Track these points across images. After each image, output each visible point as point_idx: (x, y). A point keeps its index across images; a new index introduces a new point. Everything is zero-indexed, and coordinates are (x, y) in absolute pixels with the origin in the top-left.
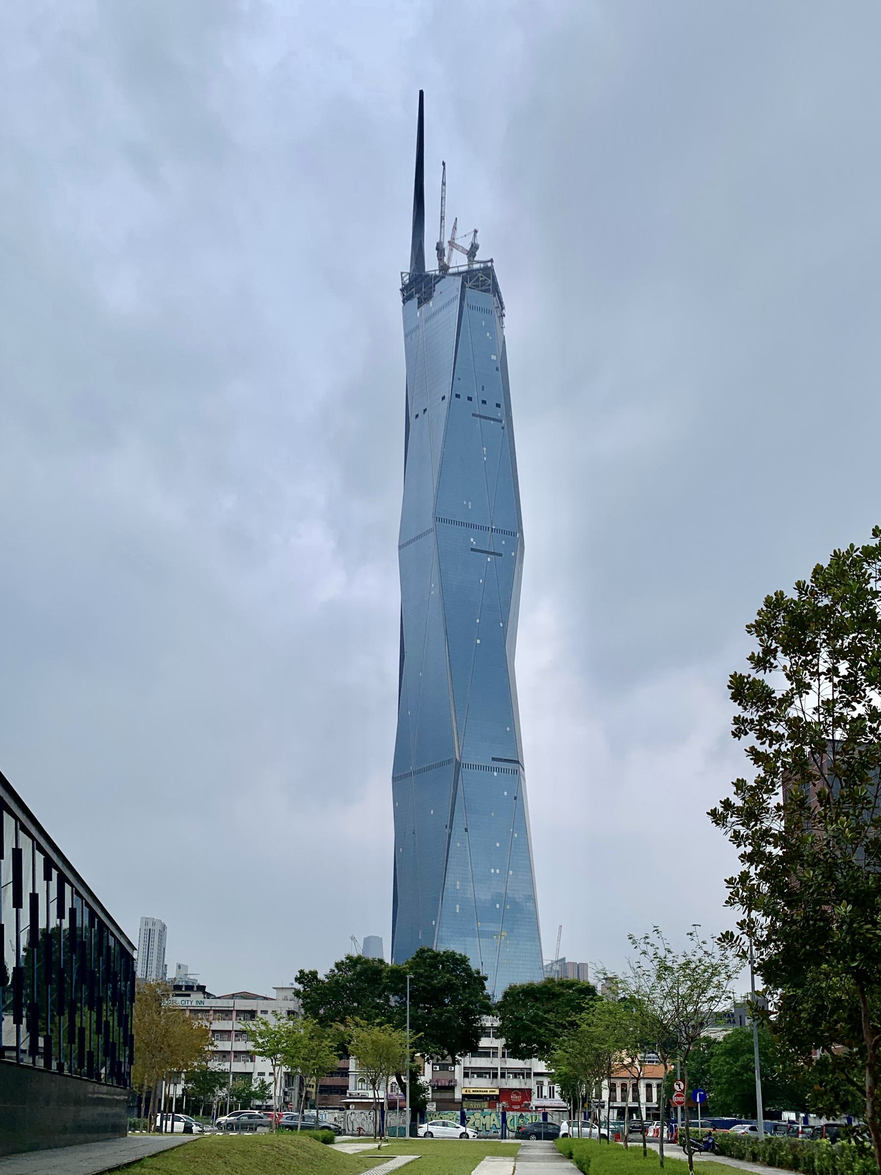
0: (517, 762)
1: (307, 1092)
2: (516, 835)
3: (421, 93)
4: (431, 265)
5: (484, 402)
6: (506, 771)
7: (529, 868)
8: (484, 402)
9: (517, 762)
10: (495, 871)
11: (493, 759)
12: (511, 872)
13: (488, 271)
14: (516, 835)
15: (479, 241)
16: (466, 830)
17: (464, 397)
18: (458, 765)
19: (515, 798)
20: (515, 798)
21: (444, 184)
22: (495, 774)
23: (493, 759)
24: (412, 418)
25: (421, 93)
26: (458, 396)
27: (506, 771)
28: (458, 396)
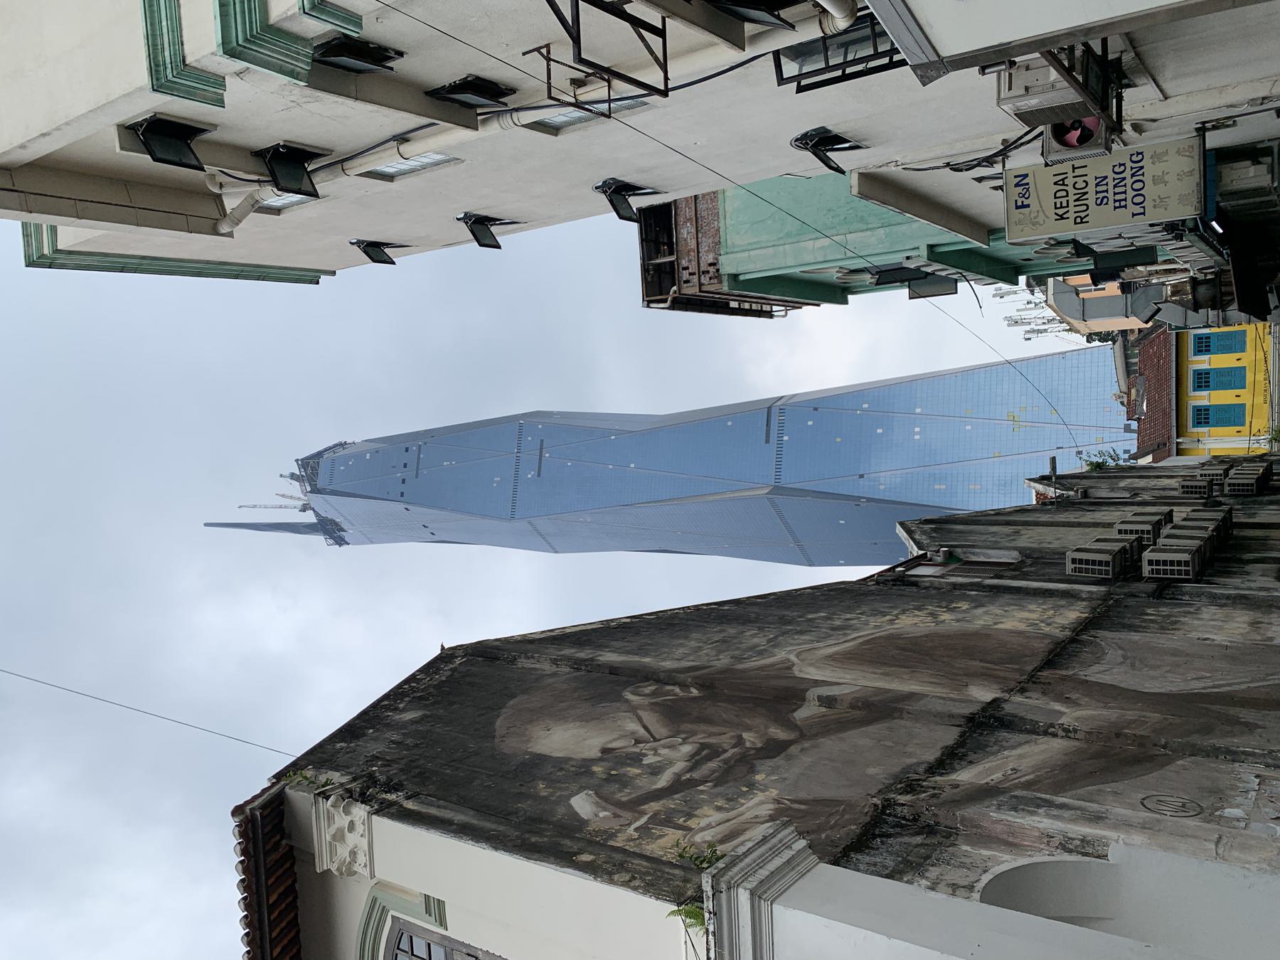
0: (769, 409)
1: (1178, 443)
2: (866, 406)
3: (206, 525)
4: (309, 517)
5: (405, 466)
6: (781, 423)
7: (506, 641)
8: (405, 466)
9: (769, 409)
10: (919, 433)
11: (767, 441)
12: (918, 410)
13: (304, 463)
14: (866, 406)
15: (287, 473)
16: (862, 476)
17: (403, 488)
18: (778, 490)
19: (816, 409)
20: (816, 409)
21: (255, 506)
22: (786, 438)
23: (767, 441)
24: (436, 538)
25: (206, 525)
26: (402, 494)
27: (781, 423)
28: (402, 494)
